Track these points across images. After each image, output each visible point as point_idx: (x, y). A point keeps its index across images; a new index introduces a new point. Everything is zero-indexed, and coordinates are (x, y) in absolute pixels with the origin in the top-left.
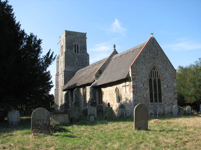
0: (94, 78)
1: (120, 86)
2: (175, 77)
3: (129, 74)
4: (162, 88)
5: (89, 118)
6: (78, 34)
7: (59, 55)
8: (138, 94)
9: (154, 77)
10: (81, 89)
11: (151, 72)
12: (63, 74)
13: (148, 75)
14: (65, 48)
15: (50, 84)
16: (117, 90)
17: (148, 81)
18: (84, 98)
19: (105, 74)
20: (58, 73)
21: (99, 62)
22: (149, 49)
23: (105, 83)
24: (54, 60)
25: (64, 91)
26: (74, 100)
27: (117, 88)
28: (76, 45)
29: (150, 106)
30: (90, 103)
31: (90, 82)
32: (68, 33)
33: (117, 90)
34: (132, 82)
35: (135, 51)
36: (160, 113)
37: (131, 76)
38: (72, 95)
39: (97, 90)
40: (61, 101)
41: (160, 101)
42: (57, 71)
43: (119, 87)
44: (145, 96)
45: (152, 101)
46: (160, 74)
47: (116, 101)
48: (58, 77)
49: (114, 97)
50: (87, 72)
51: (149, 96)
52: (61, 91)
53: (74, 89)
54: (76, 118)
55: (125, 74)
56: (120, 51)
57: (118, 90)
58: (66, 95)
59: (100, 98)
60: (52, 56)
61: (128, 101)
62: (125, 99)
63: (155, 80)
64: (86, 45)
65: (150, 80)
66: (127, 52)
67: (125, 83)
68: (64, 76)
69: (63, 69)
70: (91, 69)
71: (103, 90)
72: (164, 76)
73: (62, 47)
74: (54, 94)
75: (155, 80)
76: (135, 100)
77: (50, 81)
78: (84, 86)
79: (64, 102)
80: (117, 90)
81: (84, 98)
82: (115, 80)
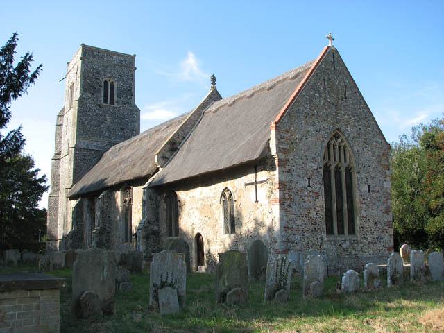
0: (156, 161)
1: (236, 185)
2: (386, 163)
3: (267, 148)
4: (357, 193)
5: (157, 300)
6: (115, 57)
7: (64, 109)
8: (295, 209)
9: (335, 160)
10: (119, 194)
11: (328, 145)
12: (72, 155)
13: (322, 155)
14: (79, 90)
15: (41, 182)
16: (226, 197)
17: (322, 171)
18: (126, 220)
19: (189, 151)
21: (169, 124)
22: (324, 80)
23: (188, 176)
24: (32, 81)
25: (72, 198)
26: (96, 224)
27: (226, 189)
28: (107, 90)
29: (325, 246)
30: (142, 234)
31: (145, 174)
32: (89, 53)
33: (227, 196)
34: (276, 172)
35: (278, 85)
36: (396, 272)
37: (274, 151)
38: (92, 211)
39: (165, 197)
40: (65, 226)
41: (352, 232)
42: (56, 148)
43: (233, 188)
44: (313, 214)
45: (330, 231)
46: (351, 152)
47: (222, 230)
48: (58, 163)
49: (216, 216)
50: (134, 149)
51: (323, 214)
52: (65, 199)
53: (98, 193)
54: (100, 297)
55: (257, 148)
56: (228, 92)
57: (231, 195)
58: (78, 212)
59: (170, 219)
60: (24, 66)
61: (263, 231)
62: (253, 223)
63: (338, 170)
64: (134, 85)
65: (327, 169)
66: (251, 92)
67: (254, 175)
68: (72, 159)
69: (70, 142)
70: (146, 141)
71: (182, 195)
72: (362, 161)
73: (72, 87)
74: (47, 208)
75: (338, 170)
76: (285, 227)
77: (33, 169)
78: (126, 186)
79: (70, 228)
80: (227, 196)
81: (126, 220)
82: (223, 165)
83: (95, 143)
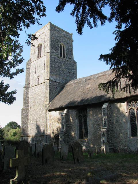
12: (48, 84)
20: (29, 84)
30: (81, 145)
42: (26, 81)
52: (44, 111)
68: (48, 87)
83: (58, 79)
